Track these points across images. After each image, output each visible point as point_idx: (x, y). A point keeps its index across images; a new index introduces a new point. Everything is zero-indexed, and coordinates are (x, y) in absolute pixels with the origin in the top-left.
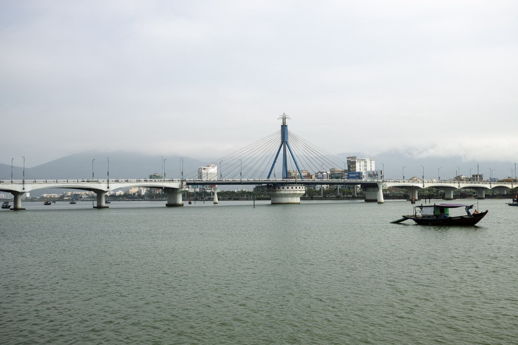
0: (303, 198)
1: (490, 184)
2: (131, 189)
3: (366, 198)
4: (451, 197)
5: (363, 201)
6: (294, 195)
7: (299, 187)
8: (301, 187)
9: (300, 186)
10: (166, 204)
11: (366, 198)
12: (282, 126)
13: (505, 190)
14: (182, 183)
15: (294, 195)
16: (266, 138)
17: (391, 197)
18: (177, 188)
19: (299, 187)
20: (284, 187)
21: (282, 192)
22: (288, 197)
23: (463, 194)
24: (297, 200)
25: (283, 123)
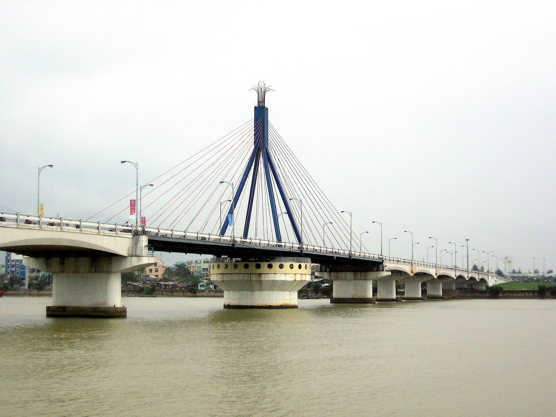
0: (303, 294)
1: (467, 272)
2: (196, 261)
3: (335, 295)
4: (105, 303)
5: (326, 302)
6: (283, 286)
7: (298, 264)
8: (303, 265)
9: (307, 262)
10: (48, 308)
11: (335, 295)
12: (255, 107)
13: (393, 280)
14: (136, 243)
15: (283, 286)
16: (290, 151)
17: (481, 292)
18: (125, 255)
19: (298, 264)
20: (273, 263)
21: (271, 277)
22: (273, 290)
23: (57, 290)
24: (291, 298)
25: (259, 102)
